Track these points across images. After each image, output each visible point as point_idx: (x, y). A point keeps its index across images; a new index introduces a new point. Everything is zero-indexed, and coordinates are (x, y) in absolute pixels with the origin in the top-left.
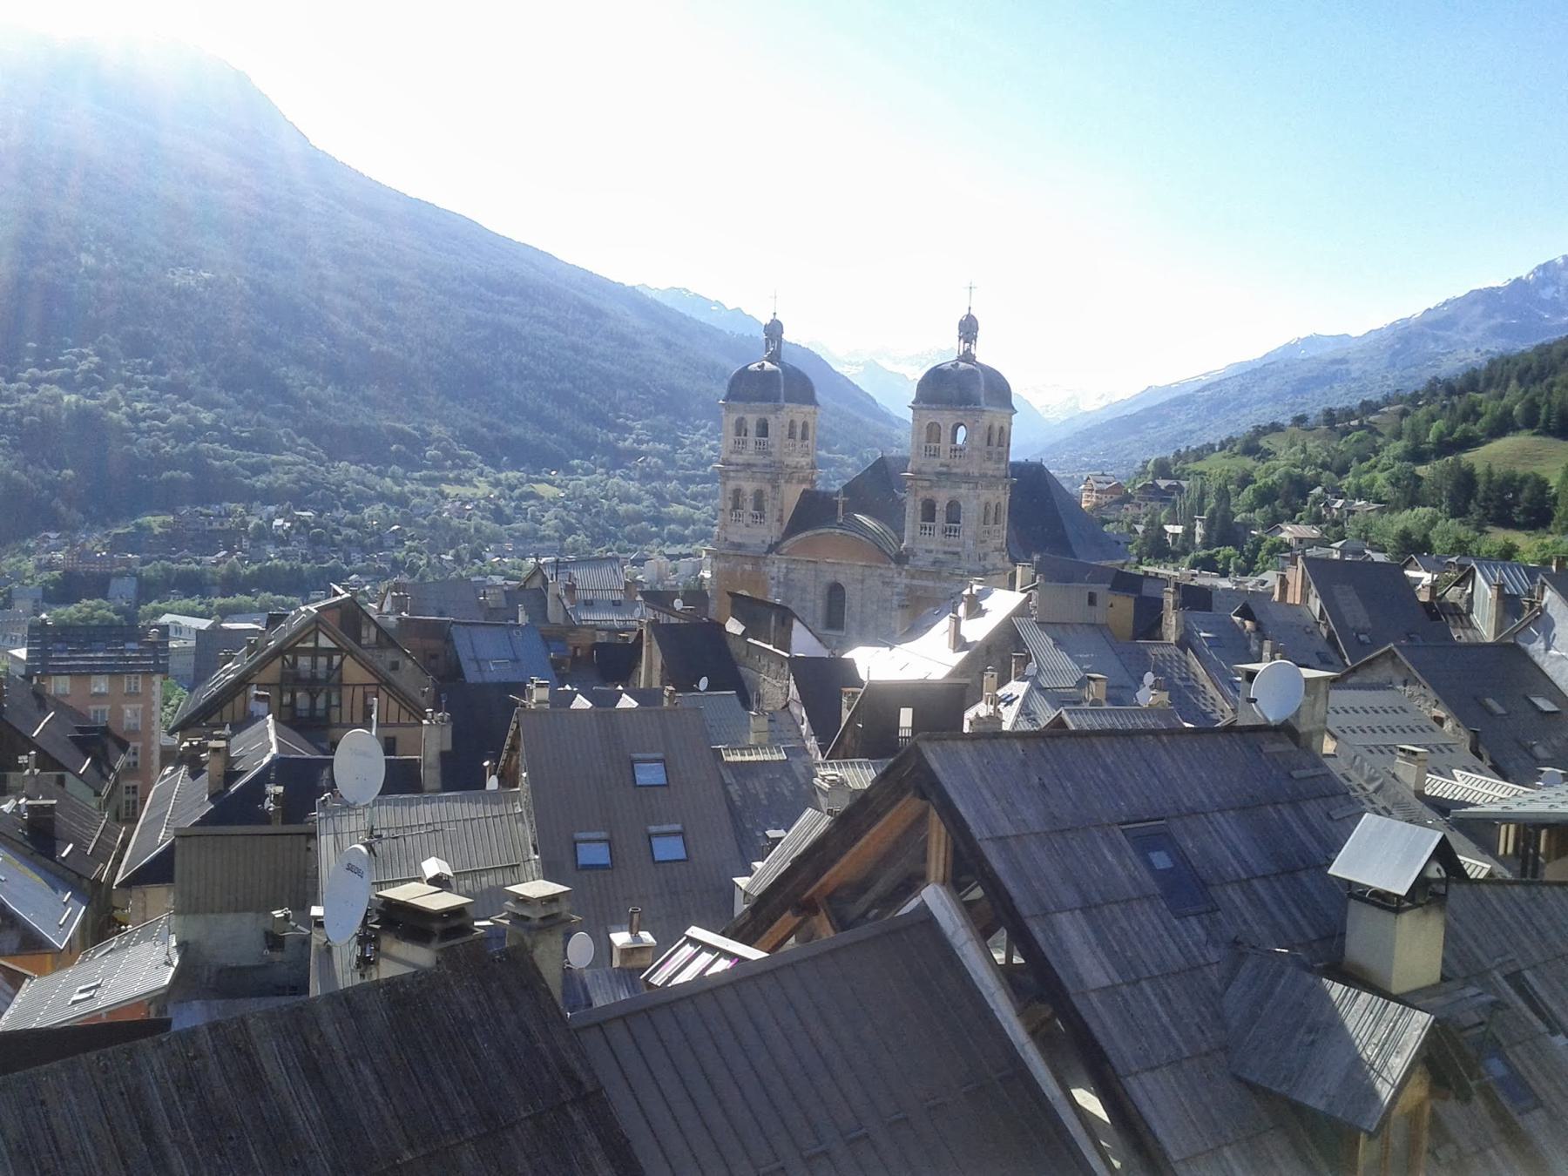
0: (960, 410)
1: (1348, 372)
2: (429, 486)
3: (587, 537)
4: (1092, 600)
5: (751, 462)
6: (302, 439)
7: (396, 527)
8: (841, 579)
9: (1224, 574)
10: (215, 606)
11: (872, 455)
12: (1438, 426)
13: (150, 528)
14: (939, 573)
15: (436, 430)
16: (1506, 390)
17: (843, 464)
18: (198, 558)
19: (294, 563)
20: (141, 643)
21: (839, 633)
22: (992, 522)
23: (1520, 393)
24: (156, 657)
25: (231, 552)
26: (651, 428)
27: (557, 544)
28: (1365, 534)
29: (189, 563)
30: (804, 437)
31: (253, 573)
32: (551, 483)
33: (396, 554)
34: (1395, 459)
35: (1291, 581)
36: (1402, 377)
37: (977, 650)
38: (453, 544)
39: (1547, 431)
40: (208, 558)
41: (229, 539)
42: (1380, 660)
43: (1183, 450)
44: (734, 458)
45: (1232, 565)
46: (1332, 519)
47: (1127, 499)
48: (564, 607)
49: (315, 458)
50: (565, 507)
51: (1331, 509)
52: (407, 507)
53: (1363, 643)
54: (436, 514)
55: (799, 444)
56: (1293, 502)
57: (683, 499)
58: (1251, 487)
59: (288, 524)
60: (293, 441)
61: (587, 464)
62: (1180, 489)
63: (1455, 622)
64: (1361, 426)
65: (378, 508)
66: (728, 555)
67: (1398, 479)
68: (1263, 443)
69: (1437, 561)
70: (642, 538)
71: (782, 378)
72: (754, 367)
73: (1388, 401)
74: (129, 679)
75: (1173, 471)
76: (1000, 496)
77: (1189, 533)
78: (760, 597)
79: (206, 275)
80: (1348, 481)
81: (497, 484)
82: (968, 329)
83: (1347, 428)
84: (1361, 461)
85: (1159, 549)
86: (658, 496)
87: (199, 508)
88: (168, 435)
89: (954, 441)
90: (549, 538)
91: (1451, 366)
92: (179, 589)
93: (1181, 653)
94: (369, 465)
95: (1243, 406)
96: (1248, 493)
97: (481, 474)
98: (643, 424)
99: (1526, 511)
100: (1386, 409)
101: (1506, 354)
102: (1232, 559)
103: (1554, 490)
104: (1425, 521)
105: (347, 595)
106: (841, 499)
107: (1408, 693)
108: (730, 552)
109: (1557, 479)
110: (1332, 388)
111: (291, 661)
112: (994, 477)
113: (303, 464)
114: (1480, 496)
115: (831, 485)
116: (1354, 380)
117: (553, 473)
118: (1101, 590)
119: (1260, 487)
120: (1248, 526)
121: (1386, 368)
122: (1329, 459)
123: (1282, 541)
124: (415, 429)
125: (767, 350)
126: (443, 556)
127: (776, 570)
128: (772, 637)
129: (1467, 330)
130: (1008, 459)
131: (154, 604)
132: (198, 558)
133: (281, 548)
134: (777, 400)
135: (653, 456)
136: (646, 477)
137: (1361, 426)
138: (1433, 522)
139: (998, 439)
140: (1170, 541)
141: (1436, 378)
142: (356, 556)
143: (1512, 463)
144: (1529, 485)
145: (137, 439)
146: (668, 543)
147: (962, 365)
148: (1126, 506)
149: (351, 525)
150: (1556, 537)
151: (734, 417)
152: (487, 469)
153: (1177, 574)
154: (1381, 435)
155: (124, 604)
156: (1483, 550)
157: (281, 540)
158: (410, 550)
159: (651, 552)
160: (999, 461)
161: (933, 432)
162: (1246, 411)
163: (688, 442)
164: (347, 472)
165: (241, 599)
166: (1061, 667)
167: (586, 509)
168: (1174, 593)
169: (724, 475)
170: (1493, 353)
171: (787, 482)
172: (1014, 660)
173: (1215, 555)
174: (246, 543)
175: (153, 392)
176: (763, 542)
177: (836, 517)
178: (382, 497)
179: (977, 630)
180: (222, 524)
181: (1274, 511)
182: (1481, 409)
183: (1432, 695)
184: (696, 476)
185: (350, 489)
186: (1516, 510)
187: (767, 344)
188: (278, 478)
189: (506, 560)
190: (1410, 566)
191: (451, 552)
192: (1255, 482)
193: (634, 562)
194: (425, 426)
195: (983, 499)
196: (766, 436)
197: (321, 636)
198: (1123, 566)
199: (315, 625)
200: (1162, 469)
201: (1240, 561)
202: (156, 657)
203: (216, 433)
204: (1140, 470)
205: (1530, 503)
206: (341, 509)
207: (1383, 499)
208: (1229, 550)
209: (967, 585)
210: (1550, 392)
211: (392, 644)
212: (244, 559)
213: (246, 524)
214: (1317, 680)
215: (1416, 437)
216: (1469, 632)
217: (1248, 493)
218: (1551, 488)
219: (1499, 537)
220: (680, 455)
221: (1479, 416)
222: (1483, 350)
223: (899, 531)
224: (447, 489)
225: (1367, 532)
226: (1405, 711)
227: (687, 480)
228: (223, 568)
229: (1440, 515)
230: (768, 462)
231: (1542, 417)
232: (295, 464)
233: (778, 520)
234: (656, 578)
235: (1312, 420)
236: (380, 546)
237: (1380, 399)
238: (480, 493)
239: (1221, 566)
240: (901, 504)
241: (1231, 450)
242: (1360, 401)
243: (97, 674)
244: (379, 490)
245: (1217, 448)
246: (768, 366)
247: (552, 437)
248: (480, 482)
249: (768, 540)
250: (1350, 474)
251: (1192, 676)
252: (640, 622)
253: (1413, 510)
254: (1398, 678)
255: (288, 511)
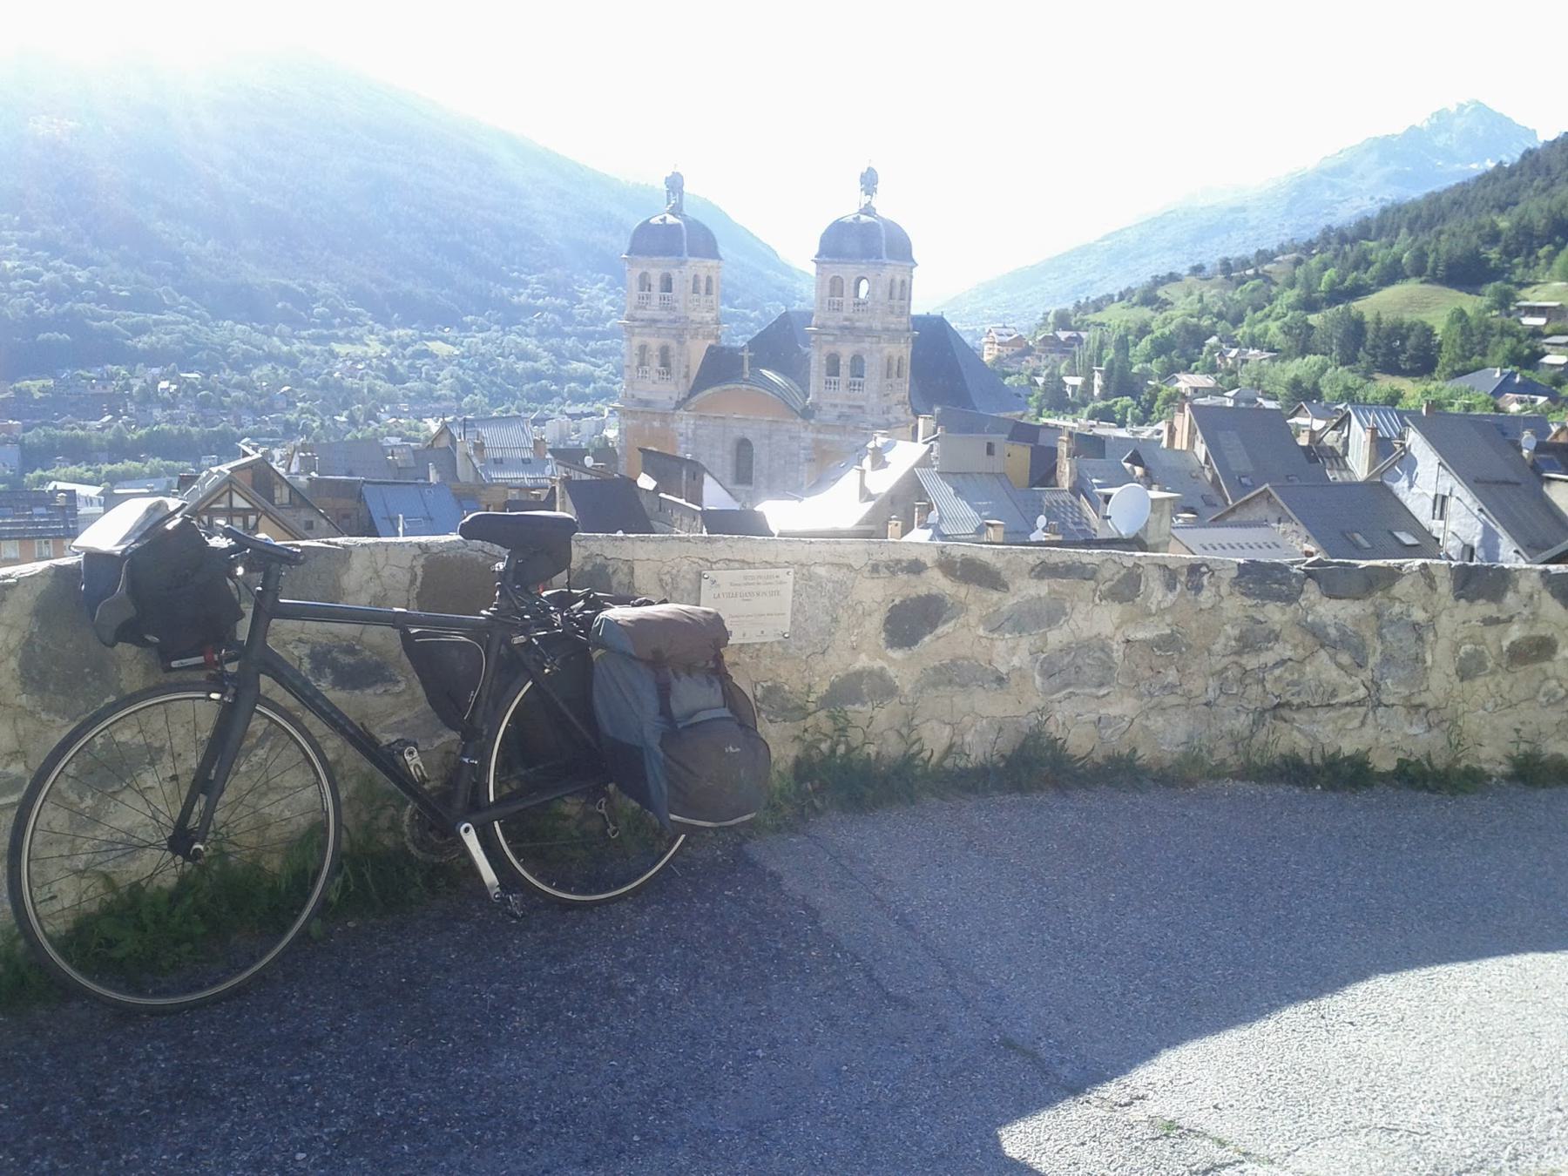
0: (862, 264)
1: (1246, 221)
2: (316, 344)
3: (485, 396)
4: (990, 450)
5: (655, 317)
6: (183, 297)
7: (286, 388)
8: (749, 435)
9: (1122, 424)
10: (103, 472)
11: (775, 310)
12: (1330, 274)
13: (29, 392)
14: (844, 427)
15: (323, 286)
16: (1396, 237)
17: (745, 318)
18: (82, 423)
19: (183, 427)
20: (48, 508)
21: (748, 488)
22: (895, 375)
23: (1409, 241)
24: (65, 522)
25: (117, 416)
26: (546, 283)
27: (454, 404)
28: (1257, 383)
29: (73, 429)
30: (708, 292)
31: (140, 437)
32: (445, 340)
33: (288, 416)
34: (1288, 308)
35: (1179, 429)
36: (1297, 224)
37: (882, 501)
38: (346, 405)
39: (1435, 279)
40: (93, 423)
41: (114, 403)
42: (1257, 500)
43: (1083, 301)
44: (639, 314)
45: (1129, 415)
46: (1226, 369)
47: (1028, 351)
48: (474, 465)
49: (199, 317)
50: (460, 365)
51: (1225, 359)
52: (296, 367)
53: (1245, 486)
54: (327, 374)
55: (703, 300)
56: (1189, 352)
57: (582, 356)
58: (1148, 337)
59: (174, 387)
60: (175, 299)
61: (481, 319)
62: (1079, 340)
63: (1332, 464)
64: (1257, 276)
65: (266, 368)
66: (636, 412)
67: (1291, 328)
68: (1161, 293)
69: (1327, 408)
70: (546, 396)
71: (685, 234)
72: (656, 220)
73: (1283, 250)
74: (39, 543)
75: (1073, 323)
76: (902, 351)
77: (1088, 384)
78: (668, 452)
79: (71, 124)
80: (1242, 331)
81: (388, 342)
82: (869, 182)
83: (1242, 277)
84: (1255, 311)
85: (1059, 401)
86: (557, 353)
87: (81, 372)
88: (43, 294)
89: (857, 296)
90: (444, 398)
91: (1346, 214)
92: (65, 456)
93: (1073, 498)
94: (254, 324)
95: (1141, 256)
96: (1145, 343)
97: (371, 332)
98: (538, 278)
99: (1411, 358)
100: (1280, 258)
101: (1397, 202)
102: (1129, 410)
103: (1439, 338)
104: (1315, 368)
105: (258, 456)
106: (746, 354)
107: (1282, 530)
108: (637, 409)
109: (1443, 327)
110: (1230, 236)
111: (206, 522)
112: (897, 330)
113: (187, 323)
114: (1369, 343)
115: (734, 341)
116: (1252, 228)
117: (447, 330)
118: (1000, 440)
119: (1157, 337)
120: (1146, 375)
121: (1282, 216)
122: (1224, 309)
123: (1177, 391)
124: (300, 286)
125: (669, 203)
126: (337, 418)
127: (684, 426)
128: (684, 491)
129: (1362, 177)
130: (909, 312)
131: (39, 472)
132: (82, 423)
133: (168, 412)
134: (681, 255)
135: (550, 312)
136: (542, 334)
137: (1257, 276)
138: (1323, 370)
139: (901, 292)
140: (1069, 392)
141: (1329, 228)
142: (247, 418)
143: (1401, 310)
144: (1416, 332)
145: (9, 300)
146: (569, 402)
147: (864, 218)
148: (1027, 358)
149: (239, 386)
150: (1440, 384)
151: (638, 271)
152: (378, 326)
153: (1076, 425)
154: (1276, 284)
155: (8, 472)
156: (1369, 397)
157: (168, 403)
158: (303, 411)
159: (552, 411)
160: (902, 314)
161: (836, 286)
162: (1145, 261)
163: (585, 296)
164: (234, 333)
165: (130, 465)
166: (957, 512)
167: (482, 367)
168: (1067, 442)
169: (630, 331)
170: (1387, 200)
171: (692, 338)
172: (916, 509)
173: (1112, 406)
174: (131, 407)
175: (22, 249)
176: (671, 398)
177: (742, 373)
178: (270, 357)
179: (883, 482)
180: (105, 387)
181: (1171, 360)
182: (1372, 257)
183: (1303, 531)
184: (595, 332)
185: (236, 348)
186: (1403, 357)
187: (668, 196)
188: (160, 339)
189: (402, 421)
190: (1300, 413)
191: (346, 413)
192: (1152, 332)
193: (535, 422)
194: (311, 282)
195: (886, 352)
196: (670, 291)
197: (235, 496)
198: (1021, 417)
199: (229, 485)
200: (1063, 321)
201: (1137, 411)
202: (65, 522)
203: (92, 292)
204: (1042, 321)
205: (1415, 350)
206: (228, 371)
207: (1276, 348)
208: (1127, 400)
209: (869, 437)
210: (1438, 240)
211: (306, 504)
212: (130, 423)
213: (129, 387)
214: (1163, 500)
215: (1309, 286)
216: (1345, 474)
217: (1145, 343)
218: (1436, 335)
219: (1386, 383)
220: (577, 310)
221: (1370, 264)
222: (1377, 198)
223: (805, 386)
224: (336, 347)
225: (1260, 381)
226: (1278, 546)
227: (586, 337)
228: (109, 434)
229: (1329, 362)
230: (672, 317)
231: (1430, 265)
232: (177, 323)
233: (685, 377)
234: (558, 437)
235: (1208, 268)
236: (270, 408)
237: (1275, 248)
238: (371, 352)
239: (1118, 417)
240: (806, 359)
241: (1129, 301)
242: (1255, 251)
243: (6, 539)
244: (266, 349)
245: (1116, 298)
246: (671, 219)
247: (443, 292)
248: (371, 340)
249: (675, 398)
250: (1245, 323)
251: (1084, 520)
252: (551, 480)
253: (1304, 358)
254: (1274, 516)
255: (173, 373)
